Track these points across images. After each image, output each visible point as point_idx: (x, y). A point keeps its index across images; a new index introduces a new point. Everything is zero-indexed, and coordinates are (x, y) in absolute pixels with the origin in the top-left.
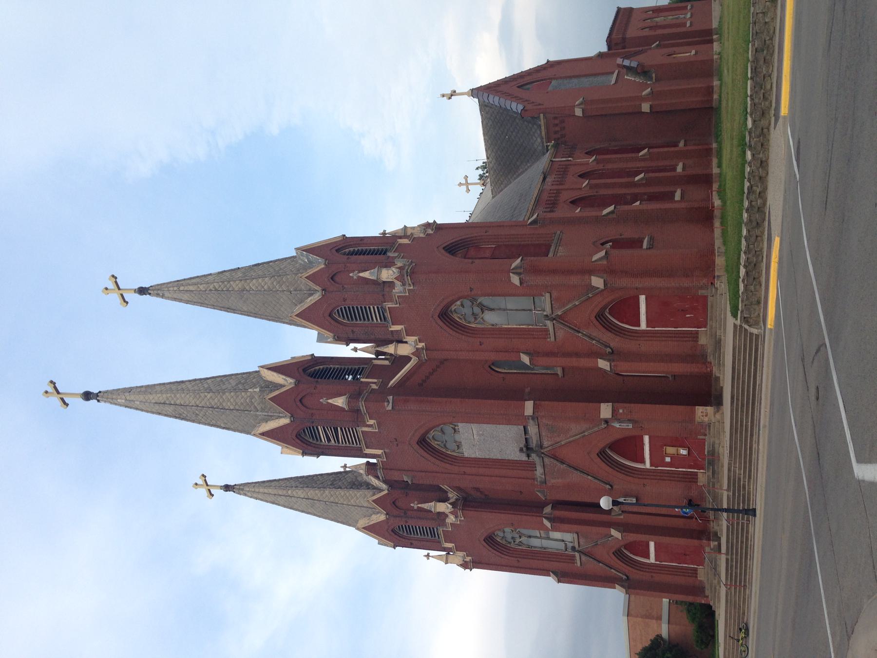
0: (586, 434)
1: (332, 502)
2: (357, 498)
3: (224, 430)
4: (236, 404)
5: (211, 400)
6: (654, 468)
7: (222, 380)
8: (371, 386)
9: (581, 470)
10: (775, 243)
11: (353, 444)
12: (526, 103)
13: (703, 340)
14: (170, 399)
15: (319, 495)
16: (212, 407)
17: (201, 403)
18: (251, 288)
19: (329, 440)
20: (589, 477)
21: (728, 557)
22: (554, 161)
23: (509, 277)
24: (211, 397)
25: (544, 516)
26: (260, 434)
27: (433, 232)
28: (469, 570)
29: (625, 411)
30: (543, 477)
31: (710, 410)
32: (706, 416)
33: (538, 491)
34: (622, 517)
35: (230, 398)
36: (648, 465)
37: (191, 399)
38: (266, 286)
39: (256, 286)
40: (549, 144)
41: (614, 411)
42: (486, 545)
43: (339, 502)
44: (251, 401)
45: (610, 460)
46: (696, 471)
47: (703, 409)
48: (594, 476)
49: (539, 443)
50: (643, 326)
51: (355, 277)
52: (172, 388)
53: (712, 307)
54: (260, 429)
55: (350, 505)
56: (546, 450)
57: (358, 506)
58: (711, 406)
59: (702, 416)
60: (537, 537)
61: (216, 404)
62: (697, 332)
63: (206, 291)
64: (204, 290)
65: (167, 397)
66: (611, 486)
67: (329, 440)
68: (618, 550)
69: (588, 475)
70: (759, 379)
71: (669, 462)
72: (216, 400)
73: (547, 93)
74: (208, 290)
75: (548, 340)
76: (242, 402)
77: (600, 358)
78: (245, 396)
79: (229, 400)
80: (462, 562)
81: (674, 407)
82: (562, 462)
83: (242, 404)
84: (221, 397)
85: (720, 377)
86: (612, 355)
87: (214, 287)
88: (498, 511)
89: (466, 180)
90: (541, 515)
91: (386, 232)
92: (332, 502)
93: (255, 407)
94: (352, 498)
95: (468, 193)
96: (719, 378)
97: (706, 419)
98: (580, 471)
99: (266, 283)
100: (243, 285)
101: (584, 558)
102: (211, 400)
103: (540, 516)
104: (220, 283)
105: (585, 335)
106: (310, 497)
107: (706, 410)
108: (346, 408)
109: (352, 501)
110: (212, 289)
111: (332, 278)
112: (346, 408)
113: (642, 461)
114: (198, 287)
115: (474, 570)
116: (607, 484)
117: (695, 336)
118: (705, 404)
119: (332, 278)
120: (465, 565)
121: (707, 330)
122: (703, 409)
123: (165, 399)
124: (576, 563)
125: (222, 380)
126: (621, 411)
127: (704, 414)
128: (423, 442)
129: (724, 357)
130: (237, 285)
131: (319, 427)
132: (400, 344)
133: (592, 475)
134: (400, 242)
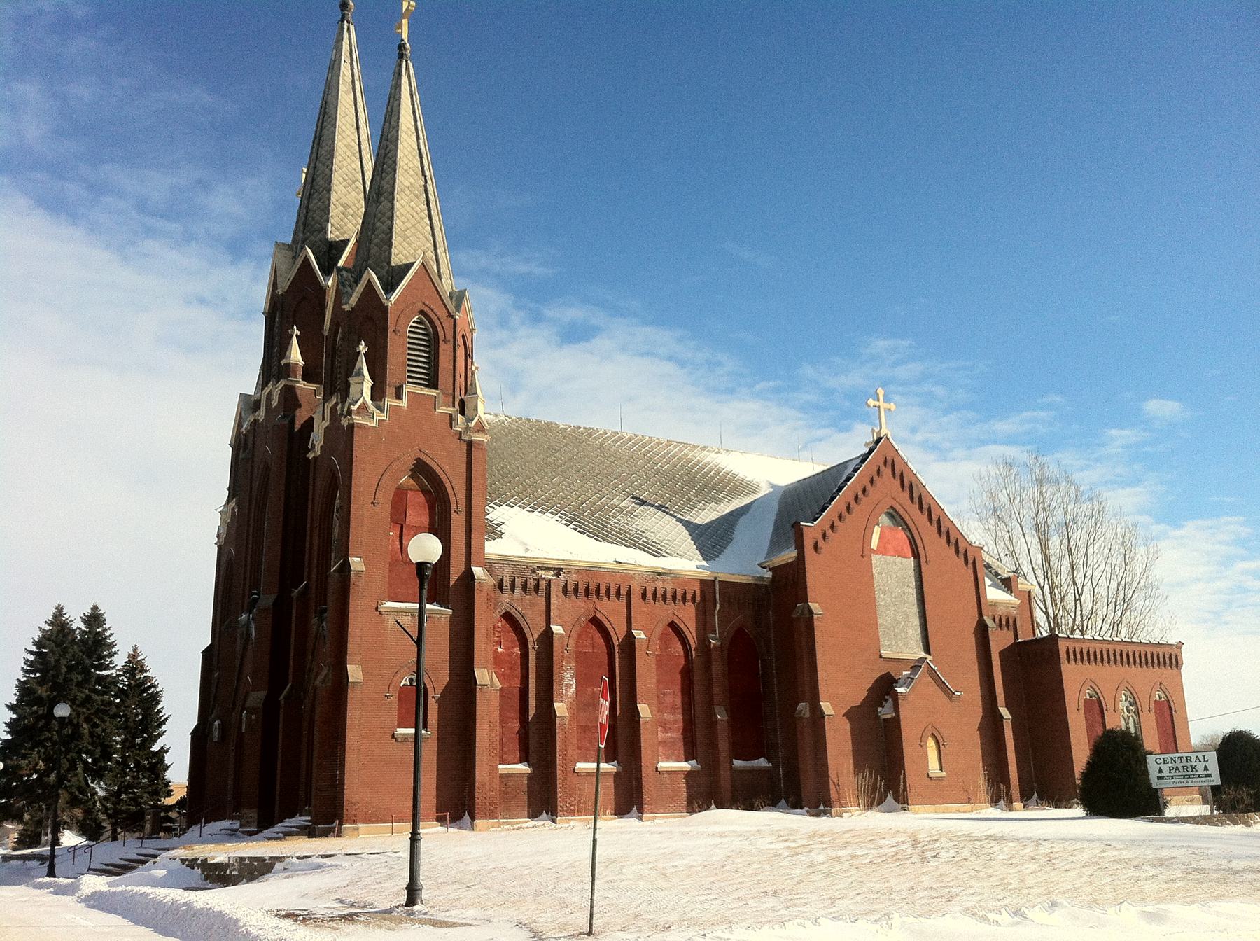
83: (313, 219)
102: (321, 176)
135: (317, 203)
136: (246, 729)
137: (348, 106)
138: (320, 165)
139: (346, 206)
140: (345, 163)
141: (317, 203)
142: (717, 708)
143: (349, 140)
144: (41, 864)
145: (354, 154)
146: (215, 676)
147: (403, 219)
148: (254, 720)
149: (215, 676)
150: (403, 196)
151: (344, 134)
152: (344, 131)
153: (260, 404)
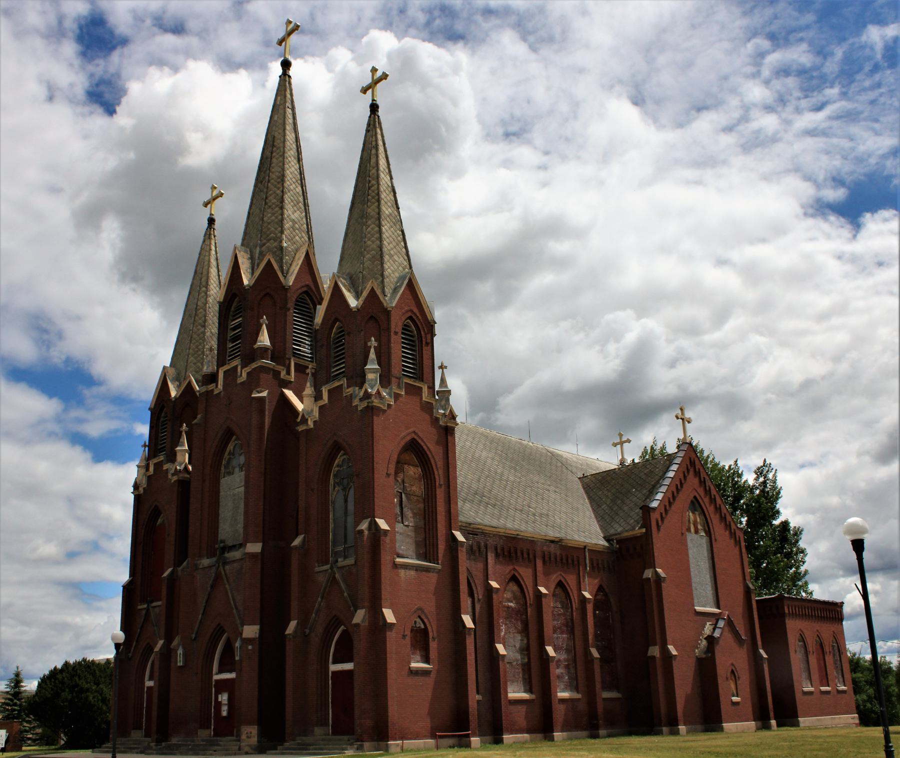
0: (235, 611)
1: (191, 337)
2: (195, 364)
3: (247, 213)
4: (269, 223)
5: (273, 195)
6: (214, 683)
7: (300, 202)
8: (283, 370)
11: (229, 356)
12: (663, 511)
13: (318, 731)
14: (278, 151)
15: (200, 321)
16: (266, 198)
17: (272, 184)
18: (369, 227)
19: (234, 329)
22: (585, 551)
23: (367, 518)
24: (277, 195)
26: (236, 254)
27: (441, 423)
28: (132, 491)
30: (201, 567)
31: (254, 740)
32: (248, 737)
33: (188, 561)
35: (276, 215)
36: (216, 677)
37: (277, 174)
38: (371, 243)
39: (370, 232)
40: (615, 541)
41: (249, 641)
43: (192, 345)
44: (271, 239)
46: (212, 727)
50: (334, 668)
51: (369, 344)
52: (291, 151)
53: (340, 740)
54: (242, 253)
55: (188, 356)
56: (221, 567)
57: (187, 366)
58: (258, 742)
59: (247, 733)
61: (270, 201)
62: (327, 725)
63: (369, 177)
64: (371, 174)
65: (279, 148)
67: (234, 329)
72: (274, 201)
73: (682, 534)
74: (370, 179)
75: (317, 565)
76: (271, 230)
77: (298, 622)
78: (277, 232)
79: (273, 214)
80: (138, 483)
82: (212, 587)
83: (269, 229)
84: (277, 206)
85: (277, 750)
86: (303, 634)
87: (373, 186)
89: (625, 442)
91: (445, 370)
92: (191, 337)
93: (264, 244)
94: (196, 358)
95: (613, 445)
96: (276, 749)
97: (244, 737)
99: (373, 242)
100: (372, 217)
101: (144, 612)
102: (273, 195)
104: (376, 192)
105: (320, 605)
106: (198, 312)
107: (254, 737)
108: (256, 346)
109: (192, 358)
110: (371, 183)
111: (372, 317)
112: (256, 346)
114: (374, 168)
115: (133, 496)
116: (196, 635)
117: (323, 723)
118: (261, 735)
119: (372, 317)
120: (136, 486)
121: (329, 735)
123: (278, 146)
124: (141, 605)
125: (300, 202)
126: (250, 647)
127: (249, 735)
128: (229, 434)
129: (292, 754)
130: (373, 210)
131: (241, 319)
132: (314, 399)
134: (423, 389)
135: (271, 217)
136: (230, 671)
137: (292, 142)
138: (410, 534)
139: (294, 222)
140: (291, 187)
141: (271, 217)
142: (503, 630)
143: (293, 169)
144: (846, 275)
145: (296, 170)
146: (165, 575)
147: (387, 240)
148: (250, 650)
149: (165, 575)
150: (386, 222)
151: (290, 164)
152: (290, 162)
153: (592, 550)
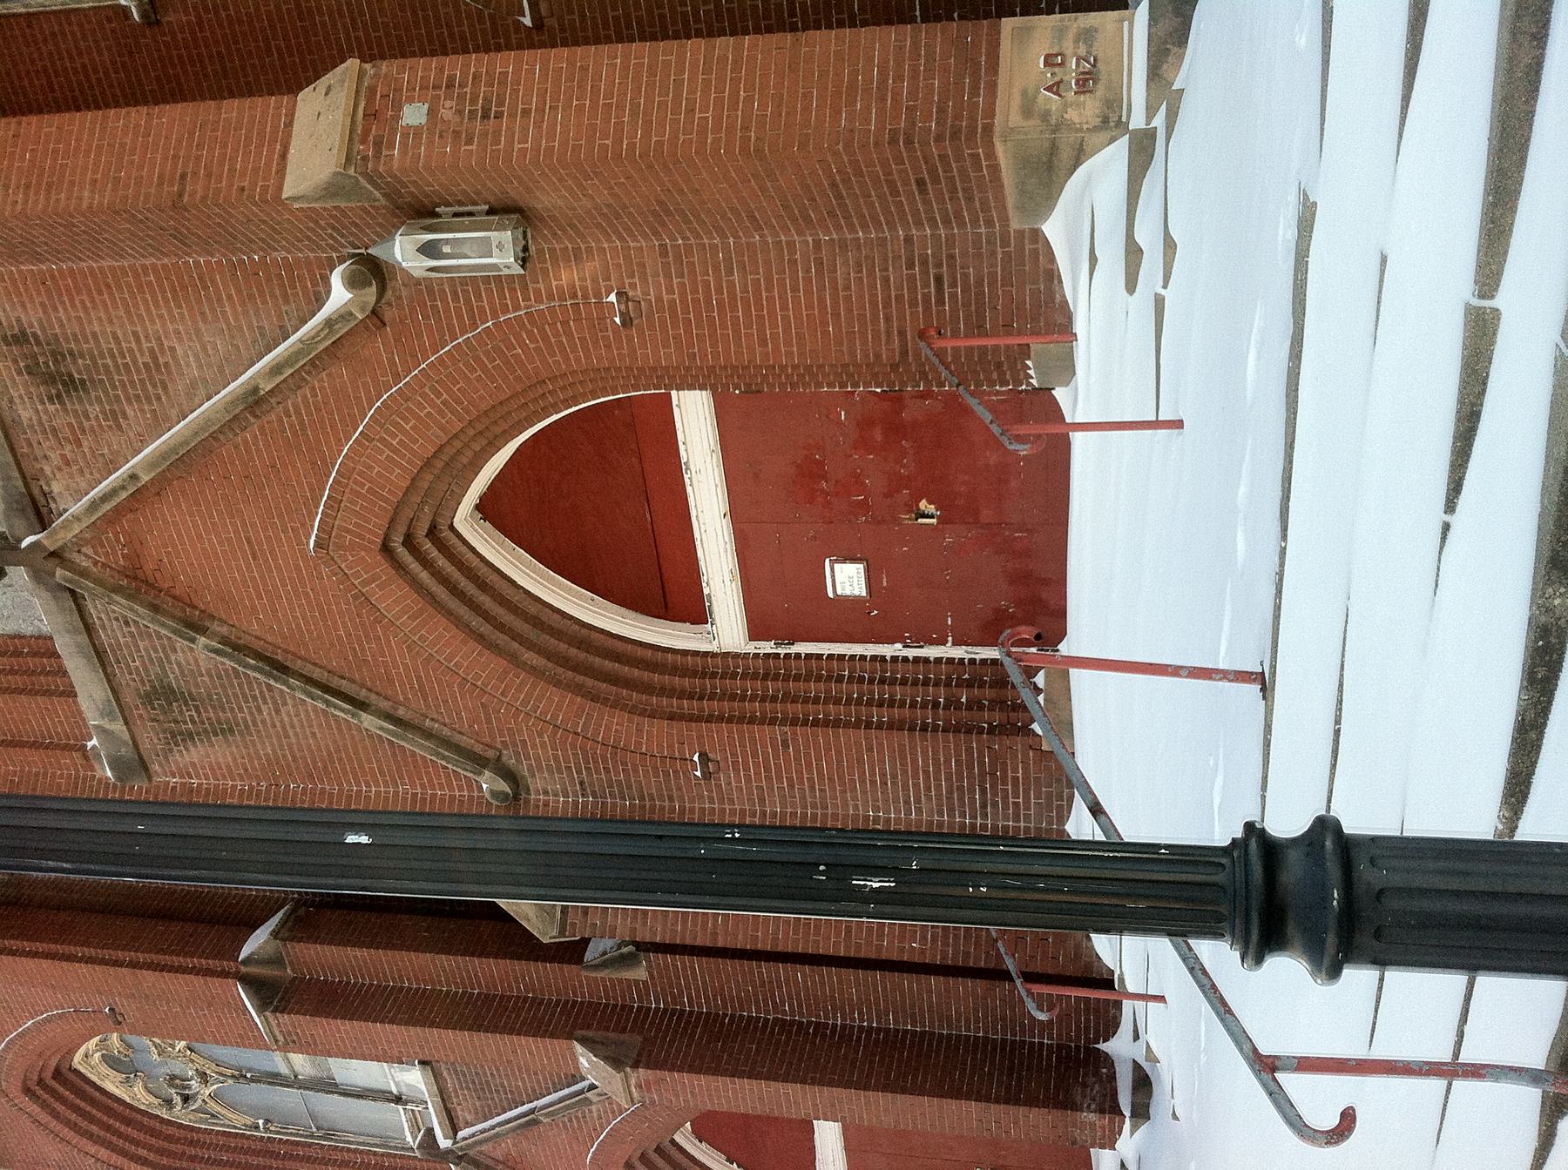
9: (317, 674)
10: (1081, 283)
20: (368, 721)
21: (573, 17)
25: (243, 969)
29: (446, 113)
34: (640, 973)
42: (45, 1117)
45: (484, 600)
47: (1061, 32)
48: (401, 712)
49: (20, 483)
59: (1055, 88)
60: (277, 1075)
66: (509, 775)
68: (659, 1150)
69: (362, 705)
70: (886, 911)
71: (853, 601)
81: (825, 43)
88: (27, 945)
90: (226, 965)
98: (309, 680)
103: (224, 974)
113: (696, 612)
116: (480, 762)
122: (1061, 32)
133: (385, 705)
